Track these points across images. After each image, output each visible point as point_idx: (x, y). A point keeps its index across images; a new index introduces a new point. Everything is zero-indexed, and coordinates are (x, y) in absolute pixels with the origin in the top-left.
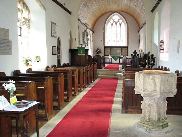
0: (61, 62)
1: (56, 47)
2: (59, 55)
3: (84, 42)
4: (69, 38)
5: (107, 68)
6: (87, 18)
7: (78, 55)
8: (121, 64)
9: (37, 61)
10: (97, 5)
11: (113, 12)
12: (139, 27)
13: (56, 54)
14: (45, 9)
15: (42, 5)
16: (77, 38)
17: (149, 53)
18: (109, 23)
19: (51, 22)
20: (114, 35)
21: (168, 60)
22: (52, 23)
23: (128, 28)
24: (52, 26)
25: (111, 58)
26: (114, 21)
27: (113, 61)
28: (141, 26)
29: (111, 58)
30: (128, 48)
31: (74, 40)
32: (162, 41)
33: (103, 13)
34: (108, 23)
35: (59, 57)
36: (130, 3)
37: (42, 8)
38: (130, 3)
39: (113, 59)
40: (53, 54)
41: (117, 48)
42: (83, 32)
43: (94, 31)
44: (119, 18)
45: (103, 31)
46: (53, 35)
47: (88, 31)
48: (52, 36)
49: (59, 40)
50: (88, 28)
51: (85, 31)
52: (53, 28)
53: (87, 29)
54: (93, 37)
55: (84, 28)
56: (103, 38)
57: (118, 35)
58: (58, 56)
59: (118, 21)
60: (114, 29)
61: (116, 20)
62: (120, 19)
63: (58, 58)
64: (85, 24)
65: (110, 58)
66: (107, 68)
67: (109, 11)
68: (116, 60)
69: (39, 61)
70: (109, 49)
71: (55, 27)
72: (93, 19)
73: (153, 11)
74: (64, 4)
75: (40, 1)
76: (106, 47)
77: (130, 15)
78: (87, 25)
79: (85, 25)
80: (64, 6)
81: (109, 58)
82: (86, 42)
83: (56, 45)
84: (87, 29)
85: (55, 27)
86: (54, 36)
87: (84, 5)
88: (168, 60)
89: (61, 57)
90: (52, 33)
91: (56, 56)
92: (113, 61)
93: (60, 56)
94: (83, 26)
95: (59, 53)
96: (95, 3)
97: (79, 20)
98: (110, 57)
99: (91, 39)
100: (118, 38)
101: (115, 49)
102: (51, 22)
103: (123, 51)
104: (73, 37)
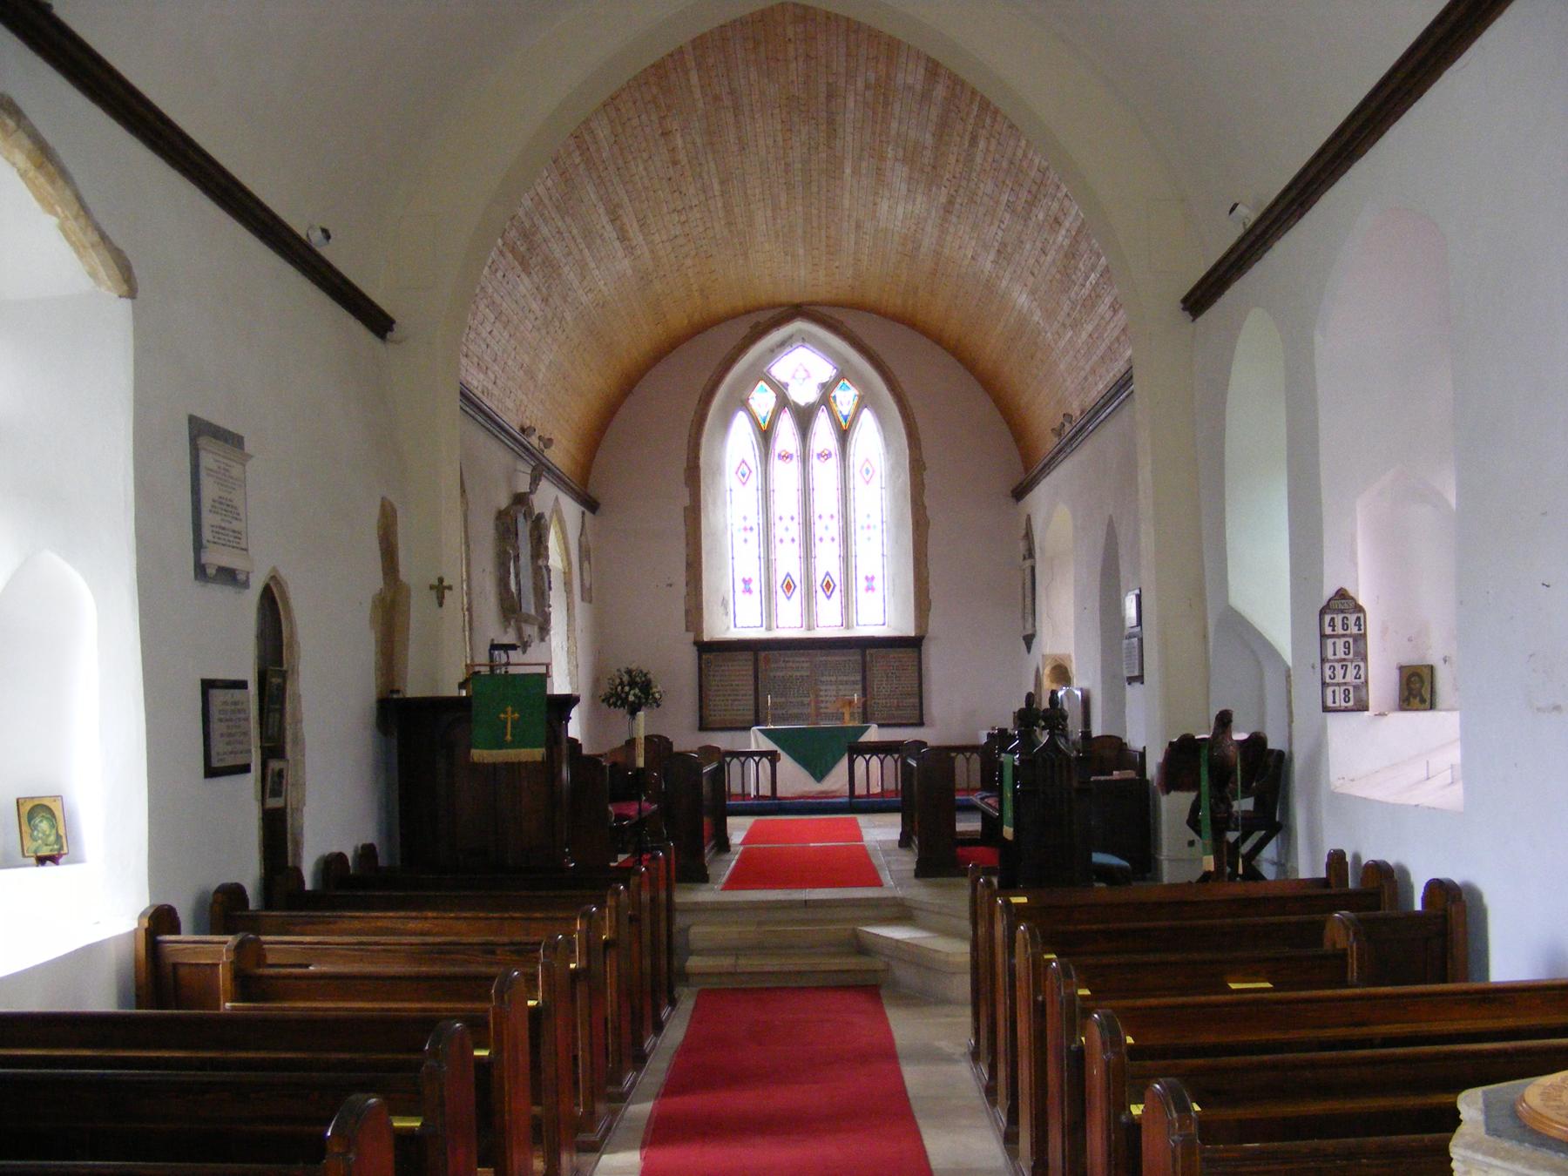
0: (298, 845)
1: (242, 685)
2: (275, 765)
3: (510, 609)
4: (376, 582)
5: (752, 872)
6: (531, 375)
7: (479, 755)
8: (873, 806)
9: (41, 861)
10: (630, 250)
11: (770, 314)
13: (245, 769)
14: (129, 284)
15: (104, 237)
16: (454, 575)
17: (1224, 720)
18: (741, 423)
19: (193, 420)
20: (787, 530)
21: (1454, 797)
22: (200, 430)
23: (917, 467)
24: (207, 460)
25: (773, 757)
26: (783, 402)
27: (793, 779)
28: (1050, 443)
29: (773, 757)
30: (934, 655)
31: (419, 605)
32: (1342, 594)
33: (678, 320)
34: (726, 422)
35: (276, 793)
36: (943, 231)
37: (93, 274)
38: (943, 231)
39: (786, 764)
40: (211, 772)
41: (820, 657)
42: (501, 515)
43: (593, 491)
44: (824, 370)
45: (686, 492)
46: (217, 557)
47: (549, 497)
48: (201, 571)
49: (272, 606)
50: (542, 469)
51: (521, 500)
52: (209, 490)
53: (535, 481)
54: (585, 553)
55: (511, 477)
56: (687, 612)
57: (826, 528)
58: (273, 784)
59: (826, 399)
60: (786, 476)
61: (804, 394)
63: (273, 803)
64: (514, 427)
65: (762, 754)
66: (752, 872)
67: (740, 304)
68: (819, 773)
69: (54, 859)
70: (741, 667)
71: (236, 470)
72: (593, 381)
73: (1199, 300)
74: (326, 234)
75: (79, 198)
76: (714, 652)
77: (937, 338)
78: (534, 440)
79: (520, 443)
80: (327, 252)
81: (751, 754)
82: (529, 606)
83: (247, 671)
84: (535, 481)
85: (236, 470)
86: (228, 576)
87: (513, 250)
88: (1454, 797)
89: (300, 785)
90: (207, 534)
91: (250, 782)
92: (793, 779)
93: (290, 777)
94: (495, 456)
95: (274, 748)
96: (610, 233)
97: (466, 397)
98: (756, 740)
99: (567, 574)
100: (827, 560)
101: (799, 666)
102: (193, 420)
103: (882, 685)
104: (412, 571)
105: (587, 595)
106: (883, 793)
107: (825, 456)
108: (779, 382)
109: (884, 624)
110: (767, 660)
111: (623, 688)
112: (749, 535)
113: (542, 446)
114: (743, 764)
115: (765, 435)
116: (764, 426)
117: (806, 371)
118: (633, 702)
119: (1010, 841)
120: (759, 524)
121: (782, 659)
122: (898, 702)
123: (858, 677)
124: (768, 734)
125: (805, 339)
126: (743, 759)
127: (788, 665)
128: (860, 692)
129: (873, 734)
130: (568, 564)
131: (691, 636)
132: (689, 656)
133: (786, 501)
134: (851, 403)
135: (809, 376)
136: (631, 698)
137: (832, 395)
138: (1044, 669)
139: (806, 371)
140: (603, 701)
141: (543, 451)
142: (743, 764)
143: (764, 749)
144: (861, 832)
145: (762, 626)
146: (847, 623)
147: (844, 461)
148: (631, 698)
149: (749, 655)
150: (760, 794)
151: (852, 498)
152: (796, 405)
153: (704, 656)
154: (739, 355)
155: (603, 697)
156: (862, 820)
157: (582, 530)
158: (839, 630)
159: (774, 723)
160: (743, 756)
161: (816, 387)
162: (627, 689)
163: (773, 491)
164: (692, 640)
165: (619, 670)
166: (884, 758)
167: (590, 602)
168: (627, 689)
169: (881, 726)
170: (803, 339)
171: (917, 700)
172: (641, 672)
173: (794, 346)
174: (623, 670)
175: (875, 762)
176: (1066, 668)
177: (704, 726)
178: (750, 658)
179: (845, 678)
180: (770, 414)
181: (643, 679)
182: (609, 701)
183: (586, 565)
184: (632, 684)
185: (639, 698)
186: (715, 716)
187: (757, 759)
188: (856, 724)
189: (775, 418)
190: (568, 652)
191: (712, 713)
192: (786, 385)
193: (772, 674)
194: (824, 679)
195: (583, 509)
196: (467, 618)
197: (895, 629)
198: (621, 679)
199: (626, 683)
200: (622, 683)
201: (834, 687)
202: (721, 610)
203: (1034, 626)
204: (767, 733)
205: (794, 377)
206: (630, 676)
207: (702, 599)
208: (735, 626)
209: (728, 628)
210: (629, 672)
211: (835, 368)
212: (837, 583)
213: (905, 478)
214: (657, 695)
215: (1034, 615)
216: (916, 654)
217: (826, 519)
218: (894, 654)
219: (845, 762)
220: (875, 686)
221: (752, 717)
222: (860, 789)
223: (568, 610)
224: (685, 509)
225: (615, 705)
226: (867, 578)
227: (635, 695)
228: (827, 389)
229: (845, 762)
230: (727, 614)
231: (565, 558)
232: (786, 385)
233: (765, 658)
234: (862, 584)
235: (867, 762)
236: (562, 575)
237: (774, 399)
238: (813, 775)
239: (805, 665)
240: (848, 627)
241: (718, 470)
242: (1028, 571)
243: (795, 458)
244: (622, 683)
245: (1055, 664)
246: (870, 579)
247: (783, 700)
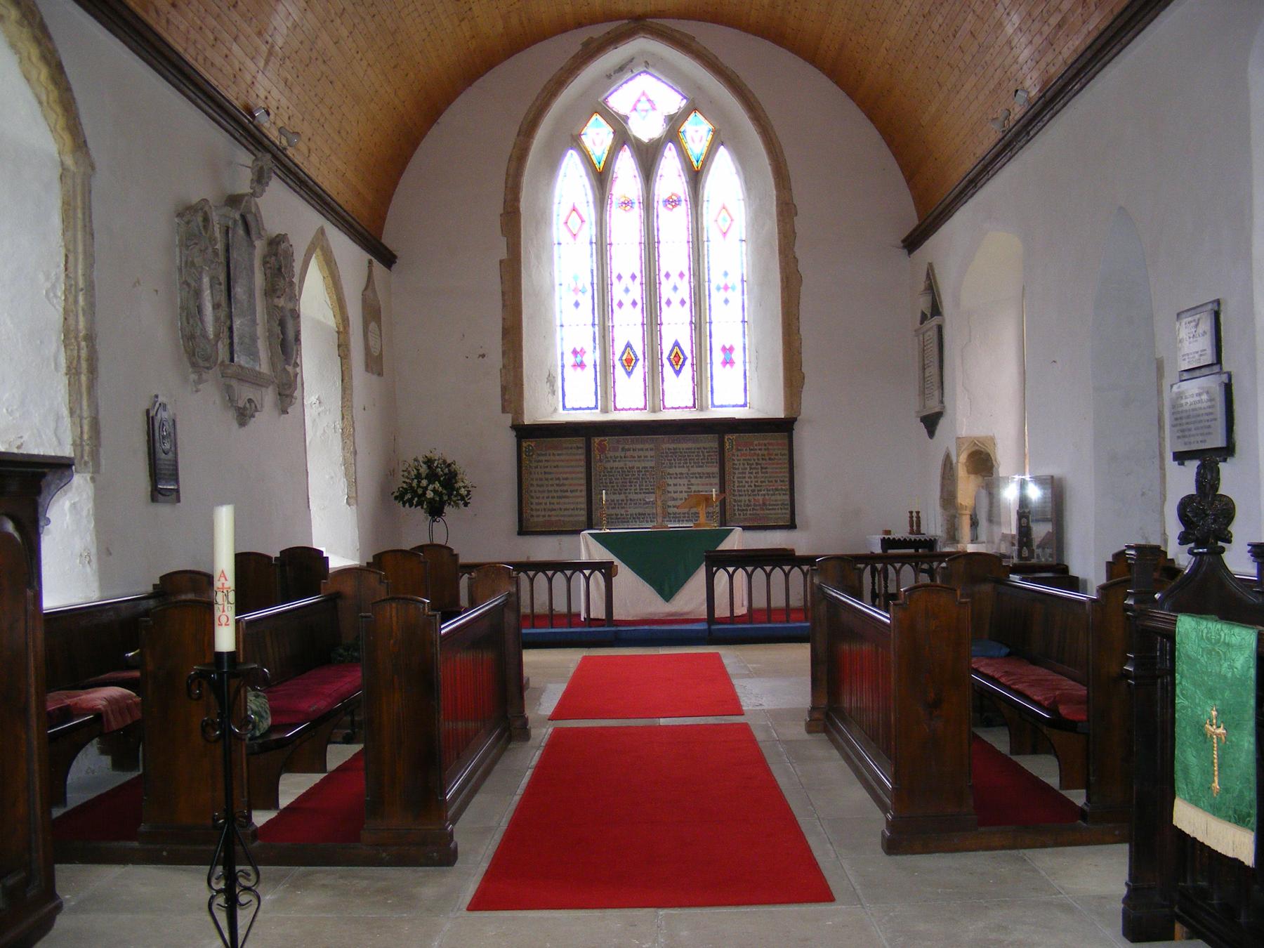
12: (920, 200)
18: (571, 164)
20: (628, 292)
23: (786, 211)
25: (607, 570)
26: (622, 137)
29: (607, 570)
30: (804, 437)
34: (553, 164)
39: (625, 577)
41: (667, 444)
43: (388, 240)
44: (672, 101)
45: (502, 243)
53: (260, 179)
56: (504, 389)
57: (675, 290)
61: (647, 128)
62: (691, 108)
65: (594, 566)
68: (667, 590)
81: (580, 567)
84: (260, 179)
98: (588, 548)
100: (676, 327)
101: (643, 453)
105: (374, 363)
106: (752, 613)
107: (672, 202)
108: (617, 114)
109: (745, 405)
110: (602, 449)
111: (419, 482)
112: (580, 297)
113: (284, 142)
114: (569, 580)
115: (601, 178)
116: (600, 166)
117: (649, 100)
118: (433, 499)
119: (1252, 869)
120: (592, 284)
121: (621, 446)
122: (763, 500)
123: (716, 470)
124: (602, 539)
125: (649, 64)
126: (568, 573)
127: (628, 453)
128: (718, 487)
129: (737, 540)
130: (343, 321)
131: (508, 419)
132: (508, 440)
133: (626, 258)
134: (704, 139)
135: (654, 108)
136: (430, 494)
137: (682, 129)
138: (958, 456)
139: (649, 100)
140: (396, 498)
141: (285, 149)
142: (569, 580)
143: (597, 559)
144: (732, 687)
145: (596, 407)
146: (698, 403)
147: (695, 193)
148: (430, 494)
149: (579, 442)
150: (592, 616)
151: (706, 252)
152: (638, 141)
153: (524, 444)
154: (568, 78)
155: (396, 494)
156: (731, 657)
157: (368, 281)
158: (691, 412)
159: (609, 526)
160: (227, 901)
161: (662, 122)
162: (424, 482)
163: (611, 244)
164: (509, 423)
165: (416, 460)
166: (753, 572)
167: (380, 374)
168: (424, 482)
169: (745, 528)
170: (646, 62)
171: (787, 497)
172: (444, 462)
173: (636, 72)
174: (421, 459)
175: (740, 575)
176: (988, 455)
177: (523, 530)
178: (581, 445)
179: (699, 470)
180: (606, 152)
181: (446, 471)
182: (403, 498)
183: (373, 325)
184: (432, 477)
185: (440, 495)
186: (538, 516)
187: (587, 572)
188: (715, 525)
189: (613, 156)
190: (342, 434)
191: (534, 513)
192: (626, 119)
193: (608, 465)
194: (672, 471)
195: (368, 256)
196: (84, 353)
197: (758, 410)
198: (418, 470)
199: (424, 475)
200: (419, 476)
201: (685, 481)
202: (547, 387)
203: (942, 402)
204: (600, 538)
205: (635, 109)
206: (429, 467)
207: (522, 372)
208: (564, 407)
209: (555, 410)
210: (429, 462)
211: (685, 98)
212: (688, 354)
213: (771, 225)
214: (463, 492)
215: (942, 389)
216: (786, 441)
217: (675, 278)
218: (757, 440)
219: (701, 574)
220: (736, 480)
221: (584, 519)
222: (722, 611)
223: (342, 381)
224: (501, 262)
225: (410, 502)
226: (724, 349)
227: (434, 491)
228: (674, 124)
229: (701, 574)
230: (554, 393)
231: (338, 312)
232: (626, 119)
233: (600, 444)
234: (718, 356)
235: (731, 577)
236: (336, 335)
237: (611, 136)
238: (661, 591)
239: (650, 453)
240: (702, 409)
241: (543, 218)
242: (933, 334)
243: (636, 206)
244: (419, 476)
245: (974, 449)
246: (727, 350)
247: (622, 496)
